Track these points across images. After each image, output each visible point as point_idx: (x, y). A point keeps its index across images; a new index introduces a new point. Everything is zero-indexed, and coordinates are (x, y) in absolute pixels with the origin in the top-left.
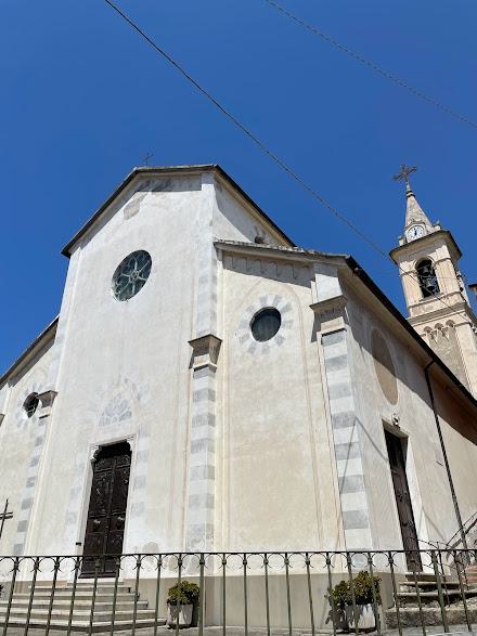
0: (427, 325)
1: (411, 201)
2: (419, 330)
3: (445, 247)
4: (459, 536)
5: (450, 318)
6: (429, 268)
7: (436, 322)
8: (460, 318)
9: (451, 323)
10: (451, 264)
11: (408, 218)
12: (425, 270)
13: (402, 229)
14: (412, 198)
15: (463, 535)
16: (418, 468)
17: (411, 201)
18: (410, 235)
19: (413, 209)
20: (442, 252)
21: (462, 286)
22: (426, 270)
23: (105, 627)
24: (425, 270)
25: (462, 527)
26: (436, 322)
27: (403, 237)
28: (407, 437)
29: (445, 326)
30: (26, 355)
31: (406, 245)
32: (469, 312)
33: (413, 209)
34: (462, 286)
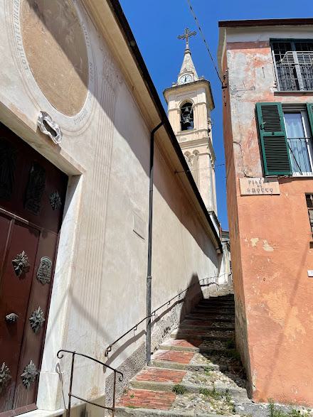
0: (196, 149)
1: (187, 57)
2: (183, 152)
3: (204, 94)
4: (143, 326)
5: (196, 149)
6: (190, 109)
7: (194, 149)
8: (204, 149)
9: (196, 153)
10: (205, 108)
11: (183, 68)
12: (186, 110)
13: (177, 74)
14: (188, 55)
15: (150, 325)
16: (84, 187)
17: (187, 57)
18: (181, 81)
19: (188, 62)
20: (200, 98)
21: (210, 128)
22: (187, 110)
23: (211, 104)
24: (186, 110)
25: (149, 315)
26: (194, 149)
27: (176, 81)
28: (77, 177)
29: (192, 154)
30: (219, 226)
31: (176, 87)
32: (210, 147)
33: (188, 62)
34: (210, 128)
